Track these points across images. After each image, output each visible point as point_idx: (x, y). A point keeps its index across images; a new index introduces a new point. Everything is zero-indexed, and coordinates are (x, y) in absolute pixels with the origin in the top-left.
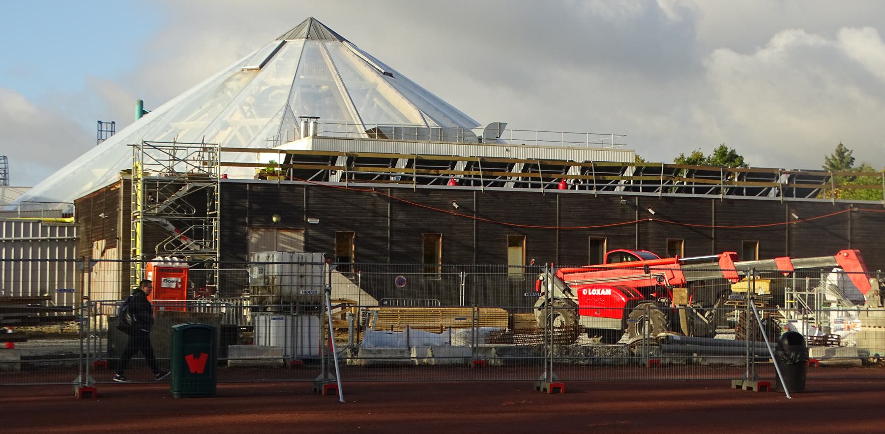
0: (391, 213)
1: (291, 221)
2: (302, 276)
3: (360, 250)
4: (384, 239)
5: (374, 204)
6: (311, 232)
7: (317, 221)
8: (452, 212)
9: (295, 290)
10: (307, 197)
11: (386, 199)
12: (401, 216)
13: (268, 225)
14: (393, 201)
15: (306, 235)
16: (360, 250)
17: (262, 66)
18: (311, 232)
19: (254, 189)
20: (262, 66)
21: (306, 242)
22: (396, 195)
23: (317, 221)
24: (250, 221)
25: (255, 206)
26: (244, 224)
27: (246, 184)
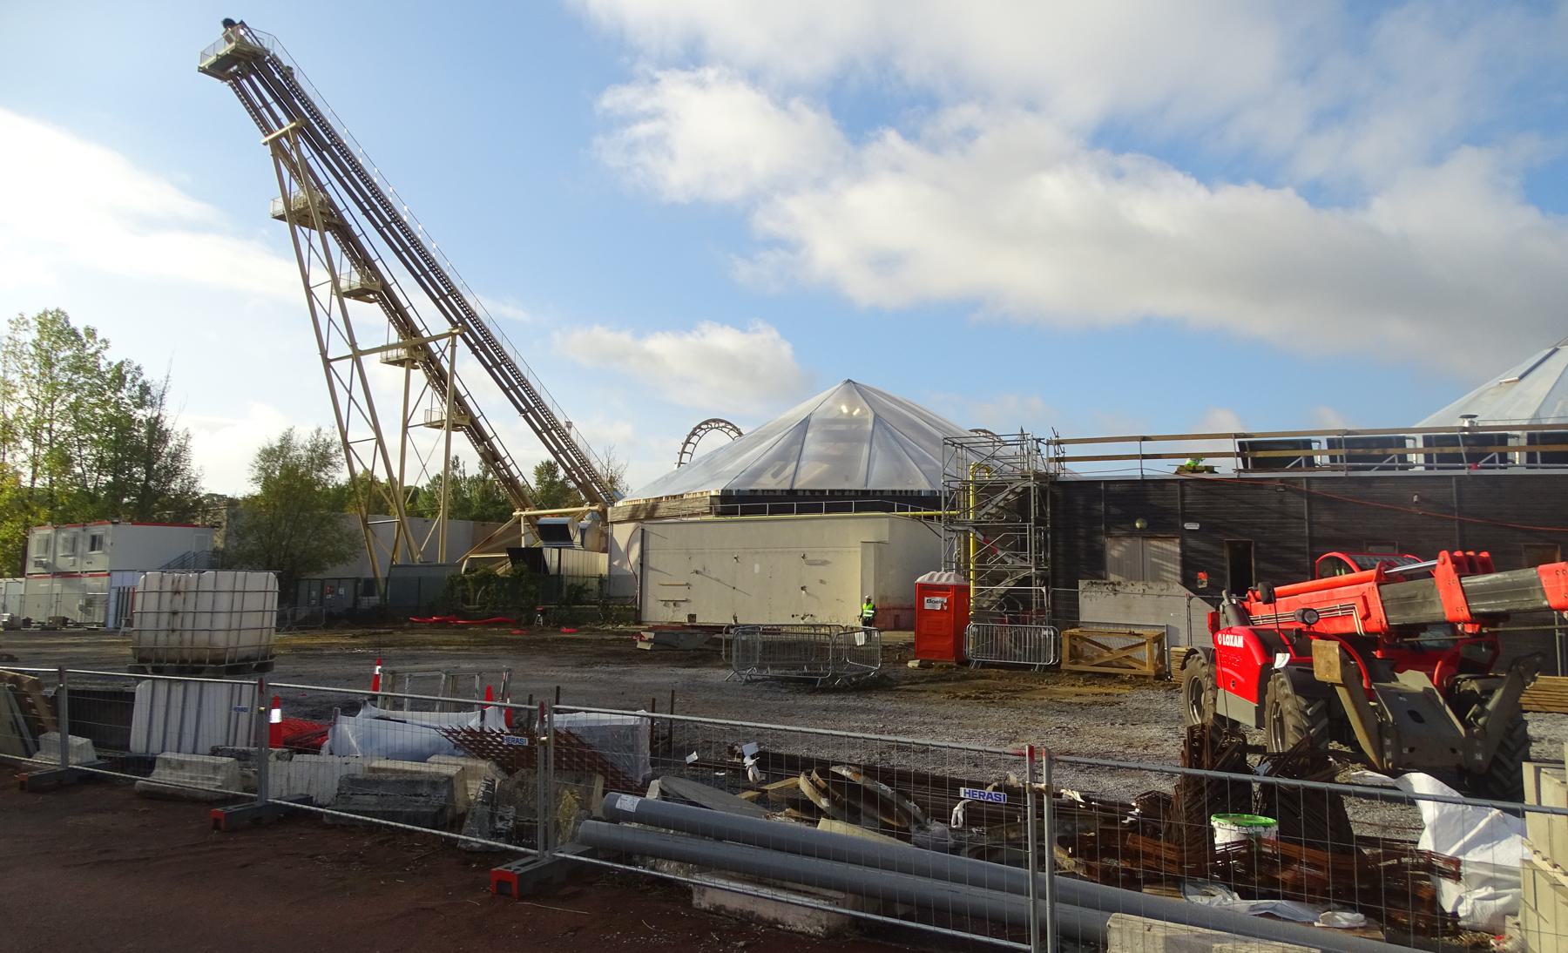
0: (1310, 513)
1: (1161, 525)
2: (175, 613)
3: (1262, 565)
4: (1297, 550)
5: (1281, 502)
6: (1191, 542)
7: (1195, 526)
8: (1414, 509)
9: (162, 636)
10: (1183, 495)
11: (1300, 493)
12: (1326, 517)
13: (1133, 533)
14: (1311, 497)
15: (1182, 545)
16: (1262, 565)
17: (1522, 377)
18: (1191, 542)
19: (1111, 488)
20: (1522, 377)
21: (1183, 554)
22: (1315, 488)
23: (1195, 526)
24: (1107, 528)
25: (1114, 510)
26: (1101, 533)
27: (1099, 482)
